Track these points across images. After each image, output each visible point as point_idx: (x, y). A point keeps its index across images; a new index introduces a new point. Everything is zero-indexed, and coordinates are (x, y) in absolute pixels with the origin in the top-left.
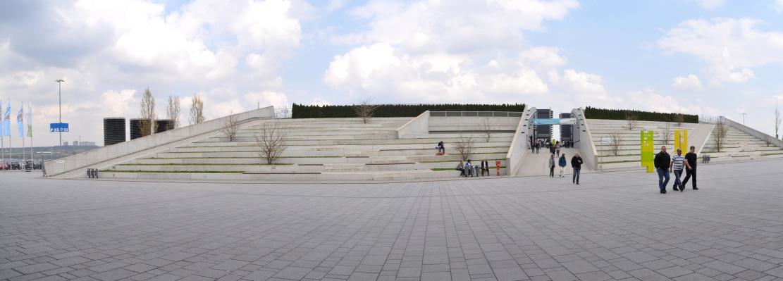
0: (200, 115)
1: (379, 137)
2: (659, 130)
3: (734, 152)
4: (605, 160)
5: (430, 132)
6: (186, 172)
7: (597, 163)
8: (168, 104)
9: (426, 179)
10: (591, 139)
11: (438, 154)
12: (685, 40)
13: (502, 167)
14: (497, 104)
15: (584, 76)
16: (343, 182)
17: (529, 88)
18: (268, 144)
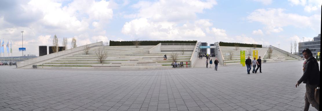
0: (75, 44)
1: (142, 53)
3: (275, 58)
5: (161, 51)
10: (222, 54)
11: (164, 59)
15: (219, 30)
16: (129, 70)
17: (199, 34)
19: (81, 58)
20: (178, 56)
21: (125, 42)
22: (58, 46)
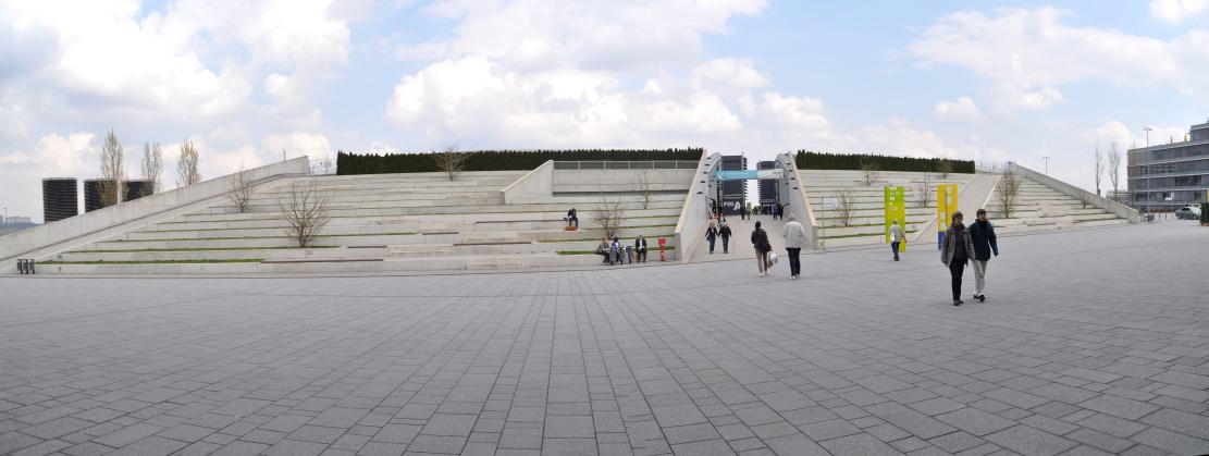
0: (193, 171)
1: (475, 202)
3: (1031, 217)
4: (828, 232)
6: (173, 261)
8: (143, 157)
9: (549, 268)
10: (807, 201)
12: (948, 43)
13: (669, 248)
14: (660, 149)
16: (419, 273)
17: (711, 120)
18: (299, 216)
21: (403, 156)
22: (124, 178)
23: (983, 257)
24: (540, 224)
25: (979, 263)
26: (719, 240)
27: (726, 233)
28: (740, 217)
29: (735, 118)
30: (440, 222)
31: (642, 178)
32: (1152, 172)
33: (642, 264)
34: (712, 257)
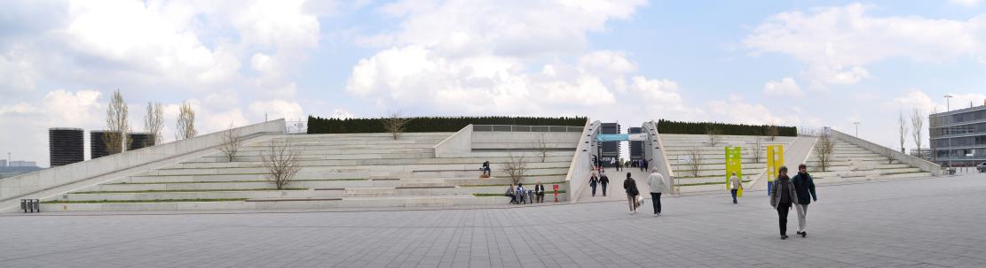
0: (190, 127)
1: (412, 156)
2: (747, 146)
3: (843, 171)
4: (682, 181)
5: (473, 150)
6: (171, 200)
7: (673, 185)
8: (146, 114)
9: (468, 207)
10: (666, 157)
11: (482, 177)
12: (777, 36)
13: (561, 192)
14: (554, 117)
15: (655, 84)
16: (368, 209)
17: (592, 98)
18: (277, 165)
19: (211, 172)
20: (529, 166)
21: (358, 120)
22: (129, 131)
23: (804, 201)
24: (462, 173)
25: (801, 206)
26: (599, 187)
27: (604, 181)
28: (615, 169)
29: (611, 95)
30: (385, 171)
31: (541, 138)
32: (953, 133)
33: (540, 204)
34: (595, 199)
